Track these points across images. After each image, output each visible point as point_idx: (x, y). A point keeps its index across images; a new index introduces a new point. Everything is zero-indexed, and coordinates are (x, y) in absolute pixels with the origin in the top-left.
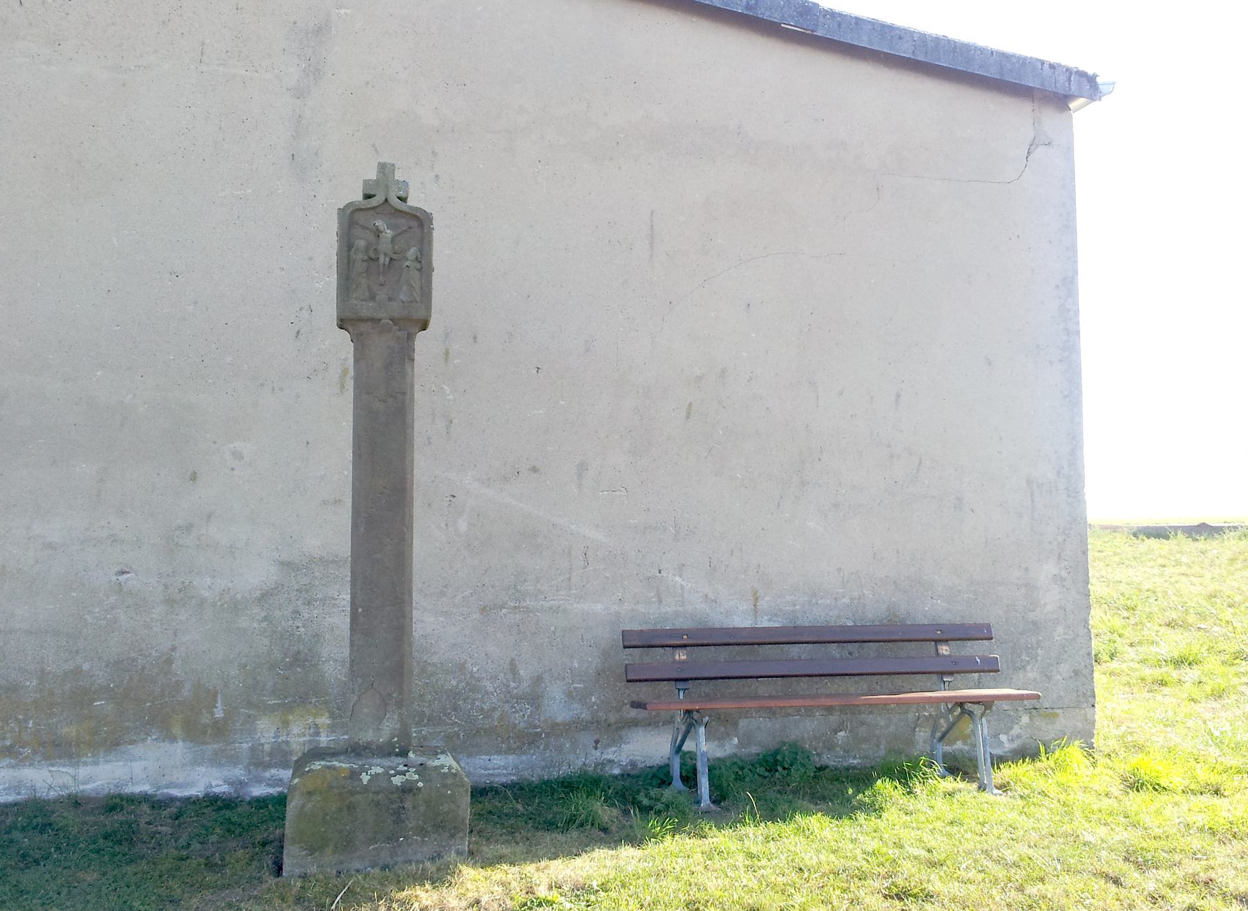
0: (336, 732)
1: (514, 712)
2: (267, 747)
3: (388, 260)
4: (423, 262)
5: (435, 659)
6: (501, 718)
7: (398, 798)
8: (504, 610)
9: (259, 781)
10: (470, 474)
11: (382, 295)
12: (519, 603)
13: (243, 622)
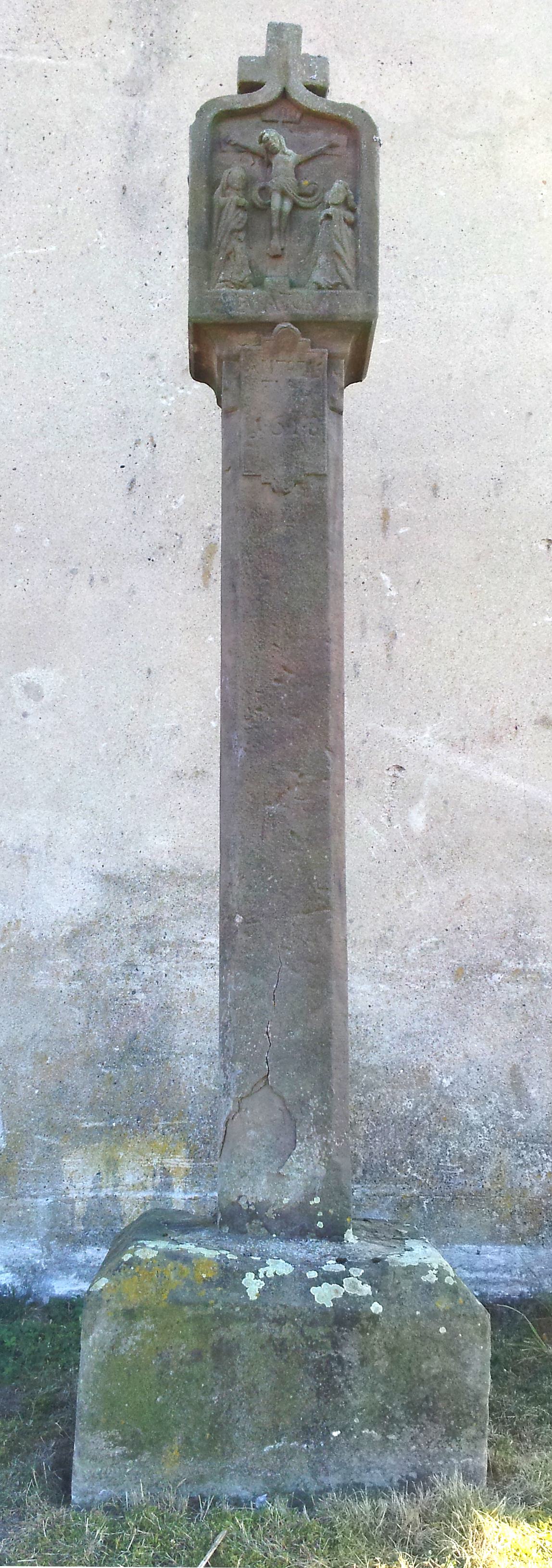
0: (199, 1185)
1: (521, 1165)
2: (79, 1206)
3: (287, 206)
4: (359, 210)
5: (374, 1059)
6: (498, 1176)
7: (327, 1336)
8: (497, 977)
9: (65, 1267)
10: (429, 728)
11: (275, 275)
12: (525, 963)
13: (41, 980)
